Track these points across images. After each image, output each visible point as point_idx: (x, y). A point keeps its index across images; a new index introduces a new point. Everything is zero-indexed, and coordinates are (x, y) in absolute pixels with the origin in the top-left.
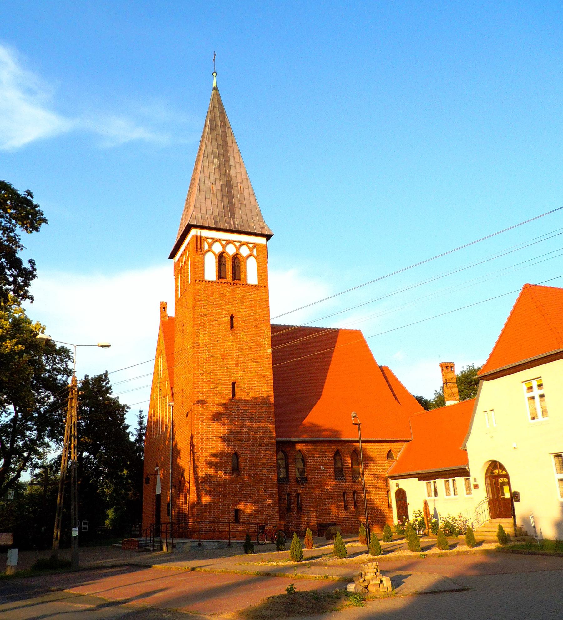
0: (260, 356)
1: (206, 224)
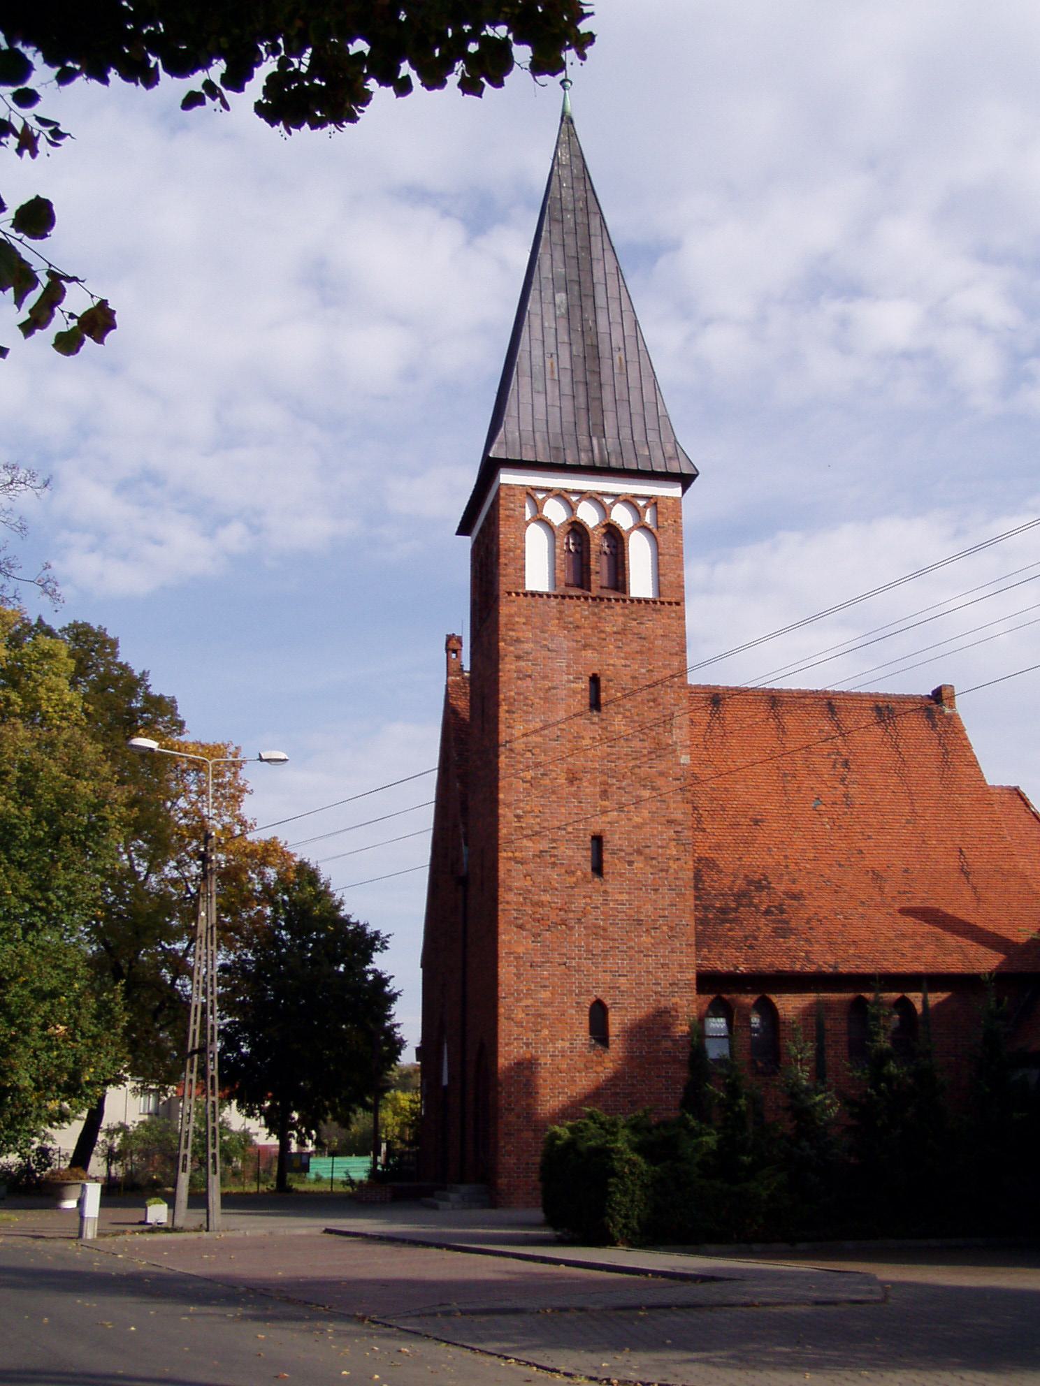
0: (662, 774)
1: (528, 456)
